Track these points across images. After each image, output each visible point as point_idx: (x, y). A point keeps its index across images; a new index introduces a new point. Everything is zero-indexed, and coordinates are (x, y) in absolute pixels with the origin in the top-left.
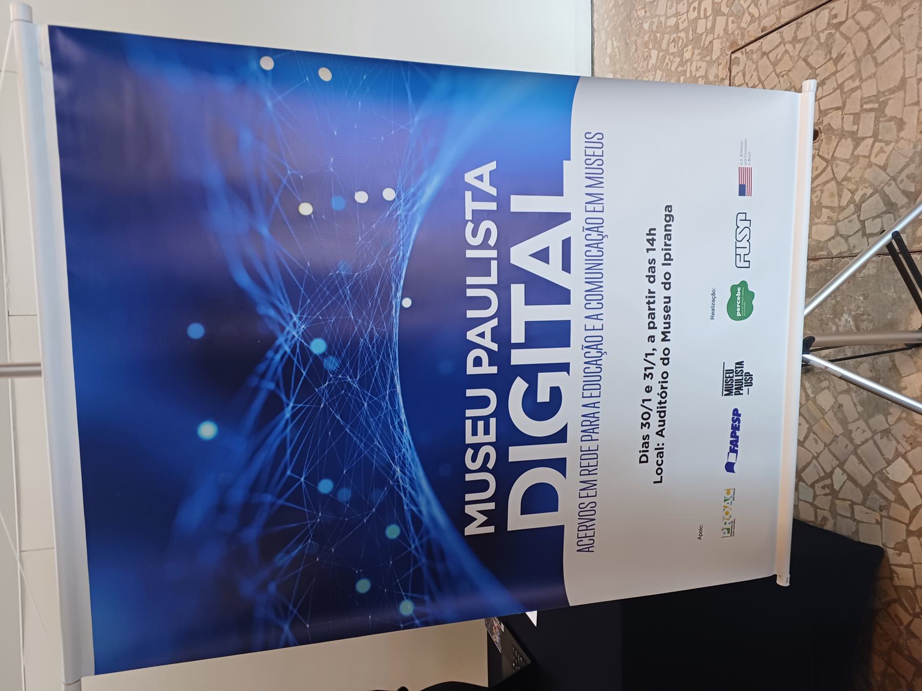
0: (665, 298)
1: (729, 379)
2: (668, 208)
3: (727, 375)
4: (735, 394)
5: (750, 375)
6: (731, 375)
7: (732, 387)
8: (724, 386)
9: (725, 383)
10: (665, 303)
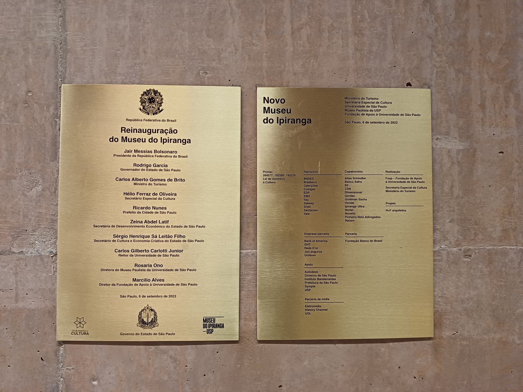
0: (145, 139)
1: (211, 320)
2: (189, 141)
3: (213, 319)
4: (203, 324)
5: (212, 332)
6: (213, 321)
7: (207, 322)
8: (208, 318)
9: (209, 318)
10: (142, 139)
